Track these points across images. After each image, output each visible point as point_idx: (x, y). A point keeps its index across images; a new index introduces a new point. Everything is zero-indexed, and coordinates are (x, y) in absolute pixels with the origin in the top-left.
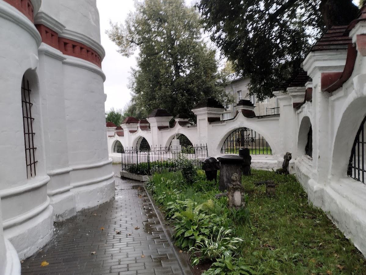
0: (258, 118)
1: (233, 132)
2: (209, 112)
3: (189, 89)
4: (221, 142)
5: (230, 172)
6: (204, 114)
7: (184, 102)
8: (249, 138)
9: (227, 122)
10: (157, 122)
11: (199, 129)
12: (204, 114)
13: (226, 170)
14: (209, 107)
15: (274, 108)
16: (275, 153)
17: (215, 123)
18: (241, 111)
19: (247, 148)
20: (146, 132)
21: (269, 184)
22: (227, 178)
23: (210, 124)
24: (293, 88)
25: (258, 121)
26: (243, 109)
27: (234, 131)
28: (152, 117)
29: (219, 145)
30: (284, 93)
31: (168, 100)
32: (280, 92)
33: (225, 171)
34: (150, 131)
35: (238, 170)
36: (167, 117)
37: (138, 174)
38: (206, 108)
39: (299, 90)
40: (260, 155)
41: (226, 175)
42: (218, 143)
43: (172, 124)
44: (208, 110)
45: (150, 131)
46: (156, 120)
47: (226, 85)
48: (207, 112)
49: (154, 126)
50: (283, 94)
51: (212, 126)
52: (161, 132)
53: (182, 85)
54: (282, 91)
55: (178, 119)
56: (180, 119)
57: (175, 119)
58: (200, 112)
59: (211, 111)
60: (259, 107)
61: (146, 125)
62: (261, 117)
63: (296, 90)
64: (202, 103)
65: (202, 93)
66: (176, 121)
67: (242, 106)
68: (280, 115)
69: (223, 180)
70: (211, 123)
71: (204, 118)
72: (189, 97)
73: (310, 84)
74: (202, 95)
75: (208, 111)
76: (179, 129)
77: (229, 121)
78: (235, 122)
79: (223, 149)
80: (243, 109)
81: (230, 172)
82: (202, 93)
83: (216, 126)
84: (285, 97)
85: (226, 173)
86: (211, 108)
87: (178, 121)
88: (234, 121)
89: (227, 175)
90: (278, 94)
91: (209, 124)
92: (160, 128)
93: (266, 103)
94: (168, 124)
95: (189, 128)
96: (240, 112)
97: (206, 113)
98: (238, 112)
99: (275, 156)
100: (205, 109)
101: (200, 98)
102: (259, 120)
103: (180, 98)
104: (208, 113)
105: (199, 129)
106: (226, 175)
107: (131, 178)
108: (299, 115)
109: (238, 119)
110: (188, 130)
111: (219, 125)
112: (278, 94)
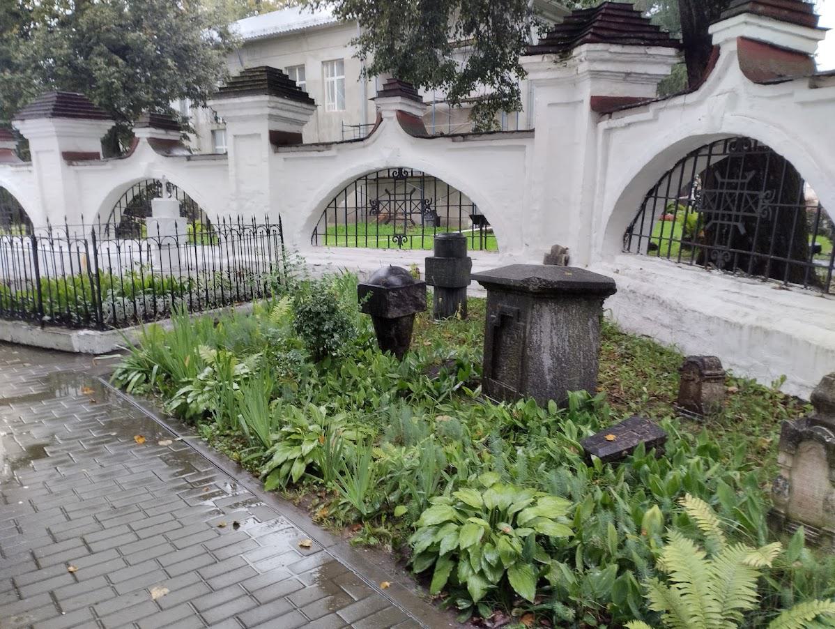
0: (453, 141)
1: (356, 182)
2: (274, 112)
3: (127, 44)
4: (315, 210)
5: (564, 334)
6: (257, 117)
7: (113, 83)
8: (395, 201)
9: (338, 150)
10: (60, 135)
11: (236, 165)
12: (257, 117)
13: (552, 324)
14: (277, 95)
15: (359, 126)
16: (505, 248)
17: (294, 149)
18: (394, 115)
19: (460, 234)
20: (13, 169)
21: (708, 372)
22: (553, 356)
23: (276, 152)
24: (600, 46)
25: (450, 150)
26: (400, 108)
27: (359, 179)
28: (39, 116)
29: (310, 219)
30: (558, 65)
31: (60, 72)
32: (546, 59)
33: (548, 330)
34: (31, 165)
35: (590, 323)
36: (94, 122)
37: (43, 324)
38: (266, 98)
39: (614, 56)
40: (347, 248)
41: (552, 343)
42: (308, 214)
43: (116, 147)
44: (273, 105)
45: (31, 165)
46: (53, 129)
47: (230, 50)
48: (267, 111)
49: (48, 151)
50: (553, 66)
51: (285, 159)
52: (77, 171)
53: (108, 30)
54: (554, 57)
55: (148, 130)
56: (152, 130)
57: (134, 131)
58: (241, 109)
59: (281, 109)
60: (317, 121)
61: (6, 147)
62: (461, 138)
63: (607, 56)
64: (244, 82)
65: (170, 62)
66: (137, 136)
67: (398, 99)
68: (536, 133)
69: (541, 364)
70: (280, 149)
71: (255, 132)
72: (130, 71)
73: (746, 23)
74: (169, 68)
75: (273, 108)
76: (151, 165)
77: (349, 145)
78: (369, 148)
79: (321, 230)
80: (399, 111)
81: (564, 334)
82: (170, 62)
83: (291, 162)
84: (558, 78)
85: (551, 337)
86: (280, 100)
87: (149, 136)
88: (364, 147)
89: (555, 344)
90: (536, 67)
91: (272, 152)
92: (71, 157)
93: (336, 110)
94: (96, 147)
95: (191, 163)
96: (390, 118)
97: (262, 115)
98: (382, 120)
99: (507, 254)
100: (263, 101)
101: (166, 76)
102: (456, 145)
103: (103, 72)
104: (271, 117)
105: (236, 165)
106: (552, 343)
107: (8, 339)
108: (609, 134)
109: (378, 140)
110: (189, 167)
111: (312, 158)
112: (536, 67)
